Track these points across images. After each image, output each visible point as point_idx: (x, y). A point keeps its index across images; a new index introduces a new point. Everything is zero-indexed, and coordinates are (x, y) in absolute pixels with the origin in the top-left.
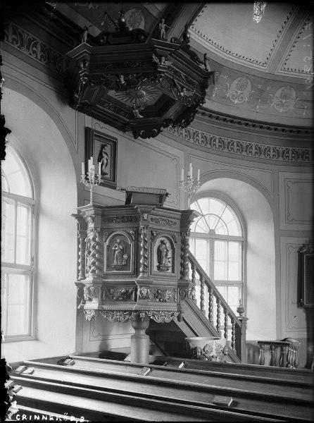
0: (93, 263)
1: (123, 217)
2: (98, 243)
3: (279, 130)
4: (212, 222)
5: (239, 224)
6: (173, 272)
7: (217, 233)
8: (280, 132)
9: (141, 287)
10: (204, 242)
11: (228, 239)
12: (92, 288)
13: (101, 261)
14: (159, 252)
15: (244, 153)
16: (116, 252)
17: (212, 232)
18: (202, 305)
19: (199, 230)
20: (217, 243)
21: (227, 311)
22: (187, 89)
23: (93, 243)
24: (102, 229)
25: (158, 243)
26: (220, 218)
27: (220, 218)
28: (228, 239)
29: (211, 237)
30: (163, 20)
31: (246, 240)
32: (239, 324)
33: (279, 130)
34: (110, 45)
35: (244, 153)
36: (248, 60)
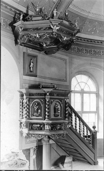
0: (26, 114)
1: (39, 94)
2: (28, 105)
3: (89, 41)
4: (83, 86)
5: (95, 86)
6: (61, 116)
7: (85, 90)
8: (8, 10)
9: (46, 125)
10: (79, 94)
11: (89, 93)
12: (25, 124)
13: (29, 112)
14: (55, 109)
15: (97, 55)
16: (36, 109)
17: (82, 90)
18: (76, 127)
19: (76, 89)
20: (84, 94)
21: (88, 128)
22: (67, 37)
23: (26, 105)
24: (29, 99)
25: (54, 103)
26: (86, 84)
27: (86, 84)
28: (89, 93)
29: (82, 92)
30: (55, 9)
31: (99, 93)
32: (94, 133)
33: (89, 41)
34: (32, 21)
35: (97, 55)
36: (95, 14)
